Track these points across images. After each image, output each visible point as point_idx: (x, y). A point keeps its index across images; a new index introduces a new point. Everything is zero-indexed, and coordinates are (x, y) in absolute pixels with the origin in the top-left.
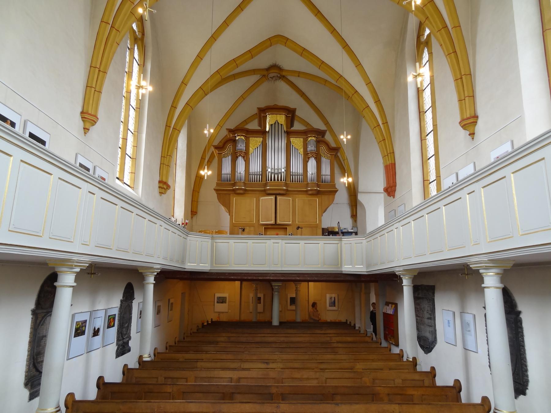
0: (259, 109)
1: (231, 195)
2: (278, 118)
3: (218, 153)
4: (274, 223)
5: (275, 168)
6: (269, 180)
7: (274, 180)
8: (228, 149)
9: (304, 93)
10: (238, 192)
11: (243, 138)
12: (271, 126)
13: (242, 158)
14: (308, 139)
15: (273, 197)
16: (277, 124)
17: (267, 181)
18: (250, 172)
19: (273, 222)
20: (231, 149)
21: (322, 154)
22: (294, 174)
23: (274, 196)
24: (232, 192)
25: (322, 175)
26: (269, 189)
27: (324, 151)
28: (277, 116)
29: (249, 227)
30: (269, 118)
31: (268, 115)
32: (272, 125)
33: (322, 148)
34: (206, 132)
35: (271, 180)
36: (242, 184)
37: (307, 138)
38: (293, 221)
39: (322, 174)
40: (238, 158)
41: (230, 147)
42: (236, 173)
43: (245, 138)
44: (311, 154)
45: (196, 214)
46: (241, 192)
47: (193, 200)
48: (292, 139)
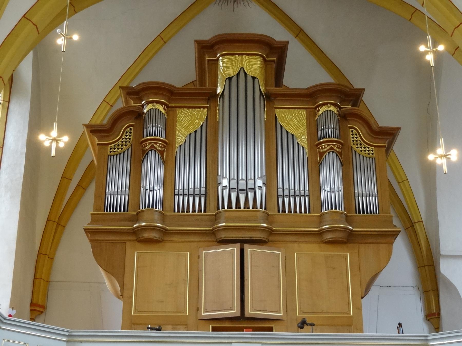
0: (197, 44)
1: (128, 244)
2: (245, 65)
3: (99, 144)
4: (238, 315)
5: (240, 178)
6: (223, 207)
7: (238, 206)
8: (124, 136)
9: (301, 30)
10: (146, 235)
11: (161, 108)
12: (228, 81)
13: (157, 154)
14: (319, 111)
15: (235, 249)
16: (242, 75)
17: (218, 209)
18: (177, 188)
19: (235, 311)
20: (132, 134)
21: (354, 147)
22: (286, 192)
23: (238, 245)
24: (130, 238)
25: (356, 194)
26: (225, 229)
27: (359, 138)
28: (242, 59)
29: (172, 325)
30: (223, 62)
31: (220, 59)
32: (230, 79)
33: (355, 132)
34: (60, 41)
35: (230, 206)
36: (156, 216)
37: (316, 108)
38: (286, 310)
39: (356, 192)
40: (147, 154)
41: (128, 130)
42: (142, 190)
43: (164, 109)
44: (328, 145)
45: (42, 312)
46: (154, 235)
47: (38, 276)
48: (278, 113)
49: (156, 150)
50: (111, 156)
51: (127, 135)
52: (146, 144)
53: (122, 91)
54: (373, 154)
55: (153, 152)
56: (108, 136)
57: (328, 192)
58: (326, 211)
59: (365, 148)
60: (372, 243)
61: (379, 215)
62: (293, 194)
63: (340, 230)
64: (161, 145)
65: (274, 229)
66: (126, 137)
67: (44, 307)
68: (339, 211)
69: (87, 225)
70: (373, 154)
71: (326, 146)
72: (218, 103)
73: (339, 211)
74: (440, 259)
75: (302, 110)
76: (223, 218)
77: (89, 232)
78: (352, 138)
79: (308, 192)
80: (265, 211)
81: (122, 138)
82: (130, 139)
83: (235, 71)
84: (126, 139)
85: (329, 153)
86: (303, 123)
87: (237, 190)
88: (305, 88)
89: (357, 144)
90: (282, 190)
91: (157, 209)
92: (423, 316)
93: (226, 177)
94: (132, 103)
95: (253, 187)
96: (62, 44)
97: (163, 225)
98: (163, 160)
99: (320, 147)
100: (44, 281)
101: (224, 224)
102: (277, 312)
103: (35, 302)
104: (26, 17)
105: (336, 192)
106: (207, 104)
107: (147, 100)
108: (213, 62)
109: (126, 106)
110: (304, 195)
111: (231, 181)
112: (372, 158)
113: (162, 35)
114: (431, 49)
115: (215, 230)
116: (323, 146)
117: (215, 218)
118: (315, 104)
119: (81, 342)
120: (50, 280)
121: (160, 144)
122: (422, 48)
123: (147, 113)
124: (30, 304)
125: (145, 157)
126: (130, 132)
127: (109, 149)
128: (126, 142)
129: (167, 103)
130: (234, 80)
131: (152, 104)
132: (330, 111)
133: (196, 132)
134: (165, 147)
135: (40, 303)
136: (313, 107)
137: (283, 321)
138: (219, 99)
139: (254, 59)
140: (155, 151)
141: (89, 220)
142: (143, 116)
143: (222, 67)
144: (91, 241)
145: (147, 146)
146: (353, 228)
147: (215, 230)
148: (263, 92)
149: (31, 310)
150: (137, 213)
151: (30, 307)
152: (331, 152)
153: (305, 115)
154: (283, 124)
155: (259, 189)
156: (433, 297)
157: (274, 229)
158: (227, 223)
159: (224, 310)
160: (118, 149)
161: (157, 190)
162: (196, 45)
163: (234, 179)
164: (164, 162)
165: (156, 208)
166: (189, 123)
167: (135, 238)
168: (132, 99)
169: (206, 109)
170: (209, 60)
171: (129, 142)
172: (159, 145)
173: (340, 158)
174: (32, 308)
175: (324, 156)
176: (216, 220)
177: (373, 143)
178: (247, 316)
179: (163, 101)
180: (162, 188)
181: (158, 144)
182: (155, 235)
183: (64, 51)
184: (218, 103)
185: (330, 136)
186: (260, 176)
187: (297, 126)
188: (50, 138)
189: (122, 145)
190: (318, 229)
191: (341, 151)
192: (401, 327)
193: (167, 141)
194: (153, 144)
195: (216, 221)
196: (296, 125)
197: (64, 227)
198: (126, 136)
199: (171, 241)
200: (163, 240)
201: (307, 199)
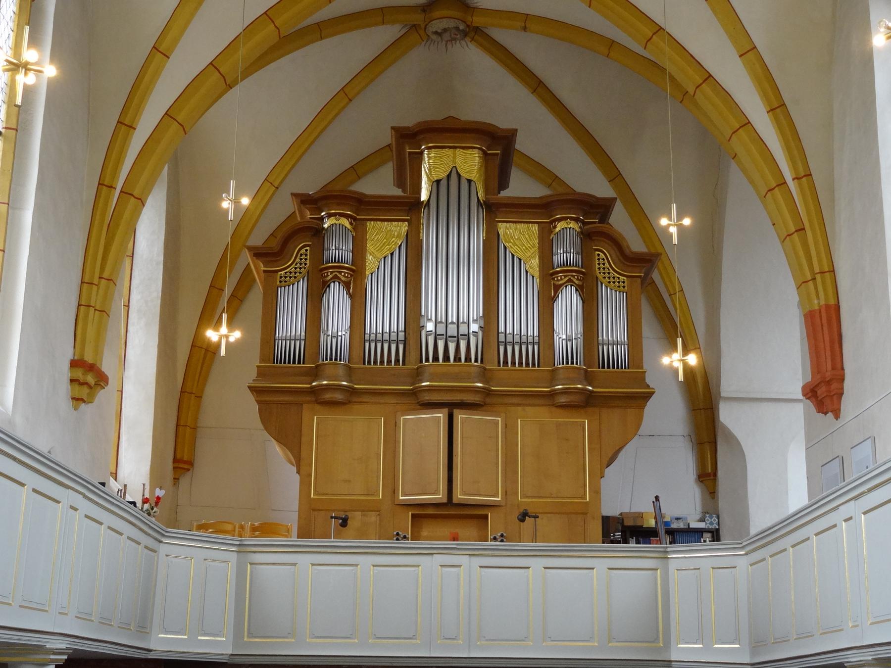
1: (305, 406)
2: (459, 162)
3: (264, 271)
4: (445, 501)
6: (427, 360)
7: (446, 358)
8: (298, 260)
9: (540, 82)
10: (328, 396)
11: (345, 222)
12: (435, 183)
13: (342, 288)
14: (555, 227)
15: (441, 416)
16: (454, 178)
17: (421, 361)
18: (368, 331)
19: (440, 496)
20: (308, 257)
22: (509, 338)
23: (446, 411)
24: (308, 399)
25: (601, 342)
26: (430, 389)
27: (607, 265)
28: (455, 155)
30: (429, 158)
31: (426, 152)
32: (438, 182)
35: (436, 358)
36: (341, 371)
37: (551, 222)
38: (506, 493)
39: (600, 338)
40: (329, 286)
41: (303, 251)
42: (322, 335)
43: (351, 224)
44: (565, 276)
45: (188, 470)
46: (339, 396)
47: (182, 423)
48: (502, 228)
49: (340, 281)
50: (281, 287)
51: (302, 259)
52: (327, 273)
53: (294, 199)
54: (624, 287)
55: (337, 283)
56: (277, 261)
57: (563, 340)
58: (560, 366)
59: (614, 278)
60: (618, 407)
61: (629, 370)
62: (519, 341)
63: (577, 392)
64: (346, 275)
65: (492, 388)
66: (301, 261)
67: (191, 463)
68: (576, 366)
69: (252, 382)
70: (624, 287)
71: (563, 277)
72: (422, 215)
73: (576, 366)
74: (720, 403)
75: (534, 225)
76: (426, 375)
77: (254, 390)
78: (598, 268)
79: (538, 338)
80: (482, 365)
81: (295, 263)
82: (306, 264)
83: (445, 172)
84: (301, 264)
85: (566, 287)
86: (533, 244)
87: (445, 337)
88: (538, 197)
89: (604, 273)
90: (504, 335)
91: (342, 362)
92: (695, 476)
93: (431, 320)
94: (308, 215)
95: (467, 333)
96: (229, 208)
97: (349, 383)
98: (350, 293)
99: (554, 278)
100: (191, 428)
101: (428, 383)
102: (493, 496)
103: (179, 456)
104: (170, 114)
105: (573, 340)
106: (408, 216)
107: (328, 212)
108: (416, 156)
109: (302, 221)
110: (532, 341)
111: (438, 325)
112: (623, 292)
113: (346, 90)
114: (675, 221)
115: (417, 390)
116: (558, 276)
117: (417, 373)
118: (551, 217)
119: (255, 553)
120: (198, 425)
121: (345, 273)
122: (664, 222)
123: (328, 228)
124: (173, 460)
125: (326, 290)
126: (306, 255)
127: (279, 278)
128: (300, 268)
129: (354, 215)
130: (444, 184)
131: (334, 217)
132: (570, 228)
133: (392, 254)
134: (351, 275)
135: (185, 458)
136: (548, 221)
137: (501, 507)
138: (423, 210)
139: (471, 154)
140: (339, 283)
141: (254, 374)
142: (322, 232)
143: (428, 165)
144: (259, 402)
145: (328, 276)
146: (593, 387)
147: (417, 390)
148: (482, 201)
149: (174, 468)
150: (316, 366)
151: (172, 464)
152: (570, 286)
153: (538, 232)
154: (507, 244)
155: (474, 335)
156: (708, 451)
157: (492, 388)
158: (432, 382)
159: (427, 494)
160: (290, 277)
161: (341, 336)
162: (393, 132)
163: (441, 322)
164: (351, 297)
165: (340, 360)
166: (383, 242)
167: (313, 399)
168: (307, 208)
169: (405, 222)
170: (410, 153)
171: (305, 268)
172: (345, 274)
173: (581, 294)
174: (177, 465)
175: (560, 290)
176: (418, 376)
177: (625, 272)
178: (456, 502)
179: (349, 213)
180: (348, 332)
181: (343, 274)
182: (339, 396)
183: (231, 220)
184: (422, 215)
185: (569, 263)
186: (475, 319)
187: (526, 247)
188: (220, 334)
189: (295, 273)
190: (549, 389)
191: (583, 284)
192: (658, 502)
193: (354, 268)
194: (336, 273)
195: (418, 378)
196: (525, 246)
197: (215, 354)
198: (301, 259)
199: (360, 402)
200: (350, 402)
201: (536, 347)
